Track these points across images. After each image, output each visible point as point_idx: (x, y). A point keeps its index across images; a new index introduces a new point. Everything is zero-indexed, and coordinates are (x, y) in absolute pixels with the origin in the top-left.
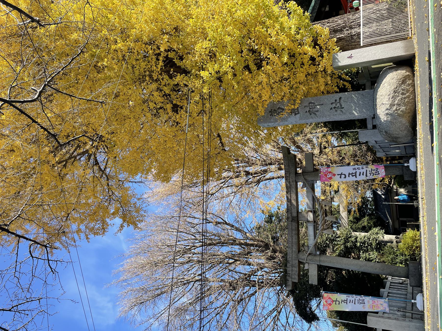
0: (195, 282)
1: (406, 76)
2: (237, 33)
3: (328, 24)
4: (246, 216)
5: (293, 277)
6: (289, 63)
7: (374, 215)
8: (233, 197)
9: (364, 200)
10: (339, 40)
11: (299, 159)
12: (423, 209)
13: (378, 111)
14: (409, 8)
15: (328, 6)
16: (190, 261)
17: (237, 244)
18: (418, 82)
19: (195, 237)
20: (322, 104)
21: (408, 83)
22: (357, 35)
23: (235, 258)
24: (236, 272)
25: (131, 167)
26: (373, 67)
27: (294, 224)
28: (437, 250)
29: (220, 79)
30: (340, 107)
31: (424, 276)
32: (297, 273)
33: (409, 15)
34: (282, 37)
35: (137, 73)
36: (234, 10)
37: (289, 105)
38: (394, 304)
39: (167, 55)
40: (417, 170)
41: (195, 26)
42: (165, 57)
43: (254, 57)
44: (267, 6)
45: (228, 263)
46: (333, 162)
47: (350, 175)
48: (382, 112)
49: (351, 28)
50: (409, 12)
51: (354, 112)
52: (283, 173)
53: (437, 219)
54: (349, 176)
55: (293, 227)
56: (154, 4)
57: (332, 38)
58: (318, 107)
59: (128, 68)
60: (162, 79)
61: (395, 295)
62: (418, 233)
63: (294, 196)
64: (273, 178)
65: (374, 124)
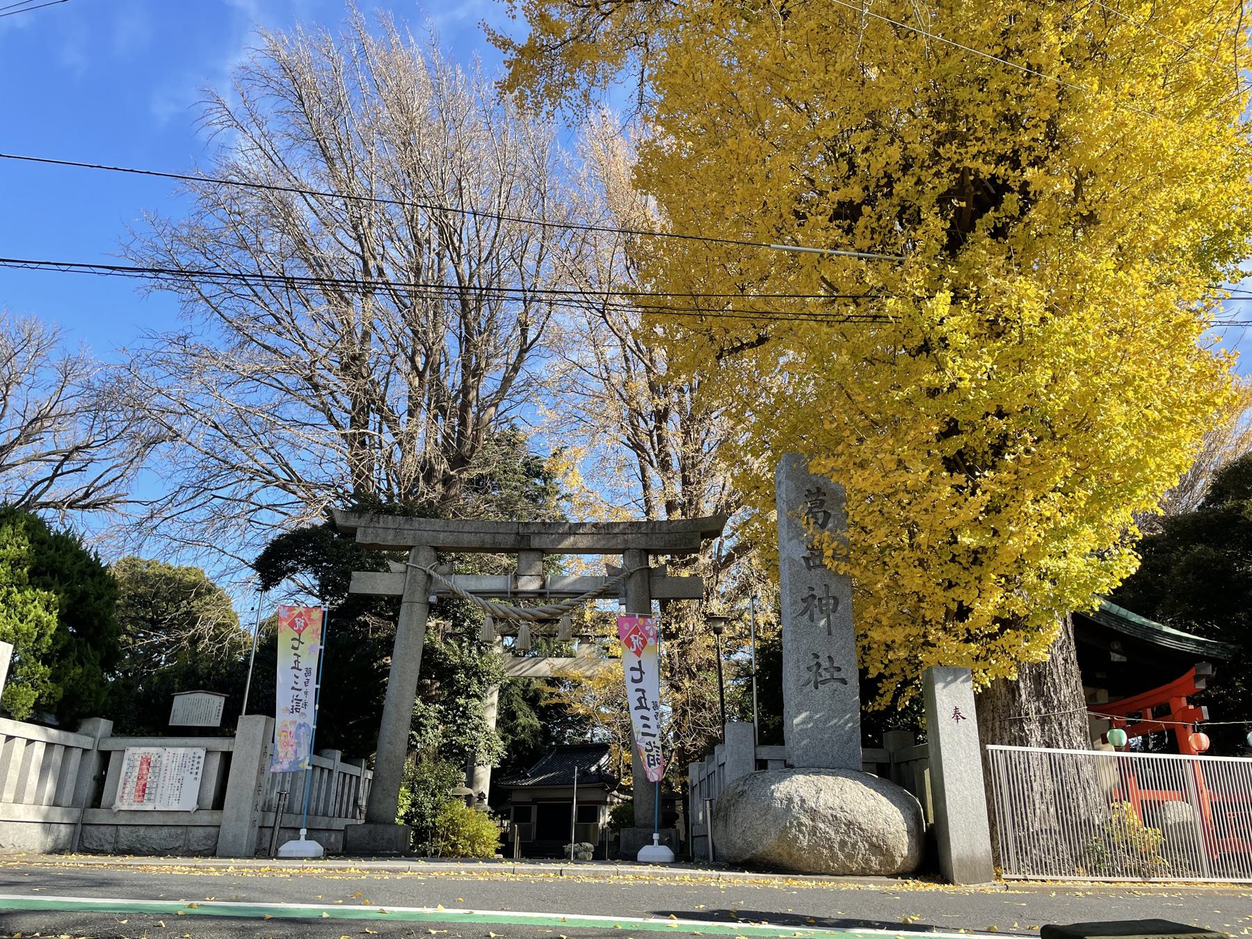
0: (363, 258)
1: (893, 856)
2: (1057, 403)
3: (1060, 660)
4: (542, 409)
5: (370, 531)
6: (957, 550)
7: (544, 743)
8: (596, 372)
9: (583, 721)
10: (1013, 688)
11: (696, 559)
12: (533, 873)
14: (1085, 878)
15: (1124, 659)
16: (419, 244)
17: (464, 382)
18: (871, 886)
19: (486, 261)
20: (830, 634)
21: (873, 858)
22: (1021, 738)
23: (429, 373)
24: (388, 374)
25: (680, 71)
26: (927, 772)
27: (510, 541)
28: (396, 909)
29: (925, 348)
30: (820, 679)
31: (364, 864)
32: (379, 541)
33: (1063, 877)
34: (1033, 533)
35: (962, 94)
36: (1130, 394)
38: (300, 783)
39: (1011, 190)
40: (640, 863)
41: (1090, 277)
42: (1005, 181)
43: (980, 451)
44: (1132, 492)
45: (414, 353)
47: (640, 694)
49: (1044, 721)
50: (1072, 878)
51: (803, 715)
52: (660, 514)
53: (476, 912)
54: (637, 690)
56: (1171, 152)
57: (1018, 668)
58: (823, 622)
59: (982, 63)
60: (938, 174)
61: (324, 787)
62: (490, 851)
63: (584, 542)
64: (646, 487)
65: (770, 764)
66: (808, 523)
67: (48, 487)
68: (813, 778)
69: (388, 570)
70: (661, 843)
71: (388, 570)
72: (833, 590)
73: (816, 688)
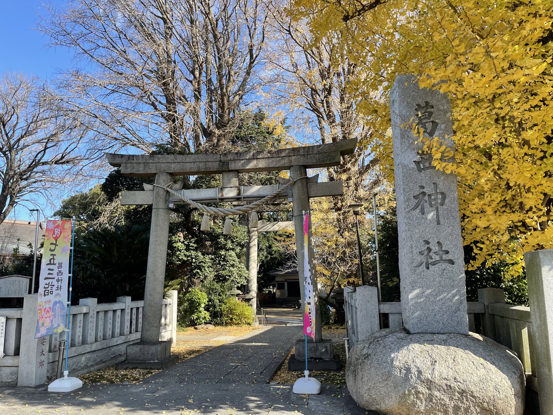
5: (129, 165)
13: (416, 347)
20: (438, 223)
26: (525, 332)
30: (430, 261)
37: (443, 148)
46: (346, 215)
48: (413, 356)
54: (51, 255)
55: (210, 164)
66: (418, 132)
67: (43, 155)
68: (428, 347)
69: (143, 190)
70: (310, 376)
71: (143, 190)
72: (441, 187)
73: (428, 268)
